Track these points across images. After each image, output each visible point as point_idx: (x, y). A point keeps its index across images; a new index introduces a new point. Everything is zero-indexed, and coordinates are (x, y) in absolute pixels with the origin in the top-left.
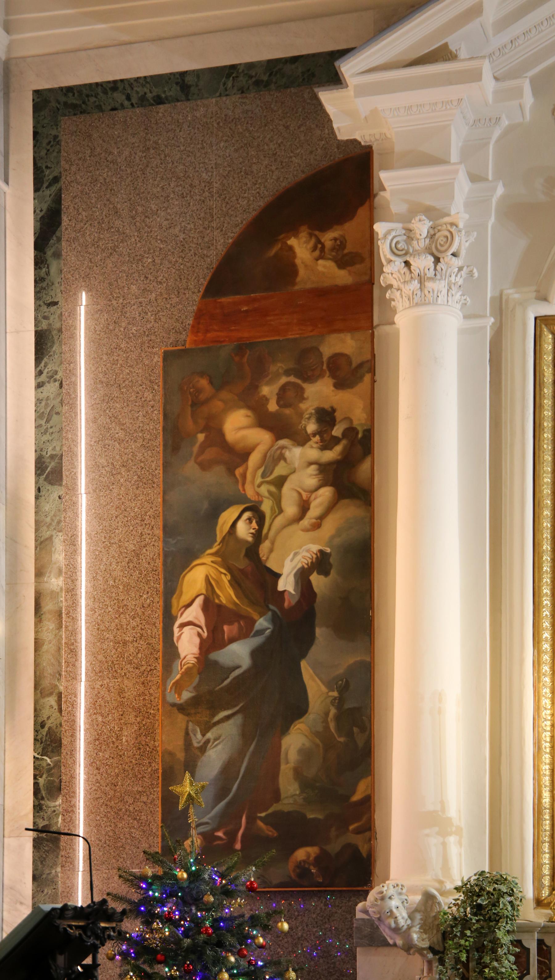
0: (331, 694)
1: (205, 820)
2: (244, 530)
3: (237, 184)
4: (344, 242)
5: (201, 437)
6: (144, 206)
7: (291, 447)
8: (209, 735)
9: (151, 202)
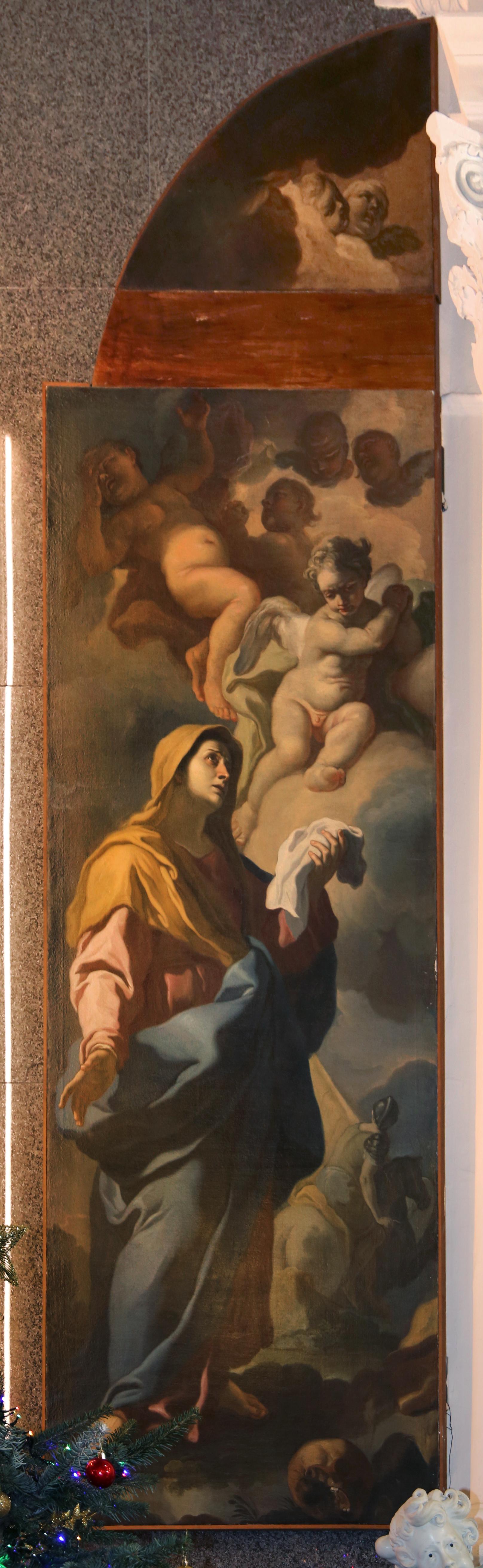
0: (364, 1127)
1: (131, 1378)
2: (203, 778)
3: (191, 70)
4: (384, 203)
5: (121, 576)
6: (15, 92)
7: (289, 614)
8: (138, 1201)
9: (30, 85)
